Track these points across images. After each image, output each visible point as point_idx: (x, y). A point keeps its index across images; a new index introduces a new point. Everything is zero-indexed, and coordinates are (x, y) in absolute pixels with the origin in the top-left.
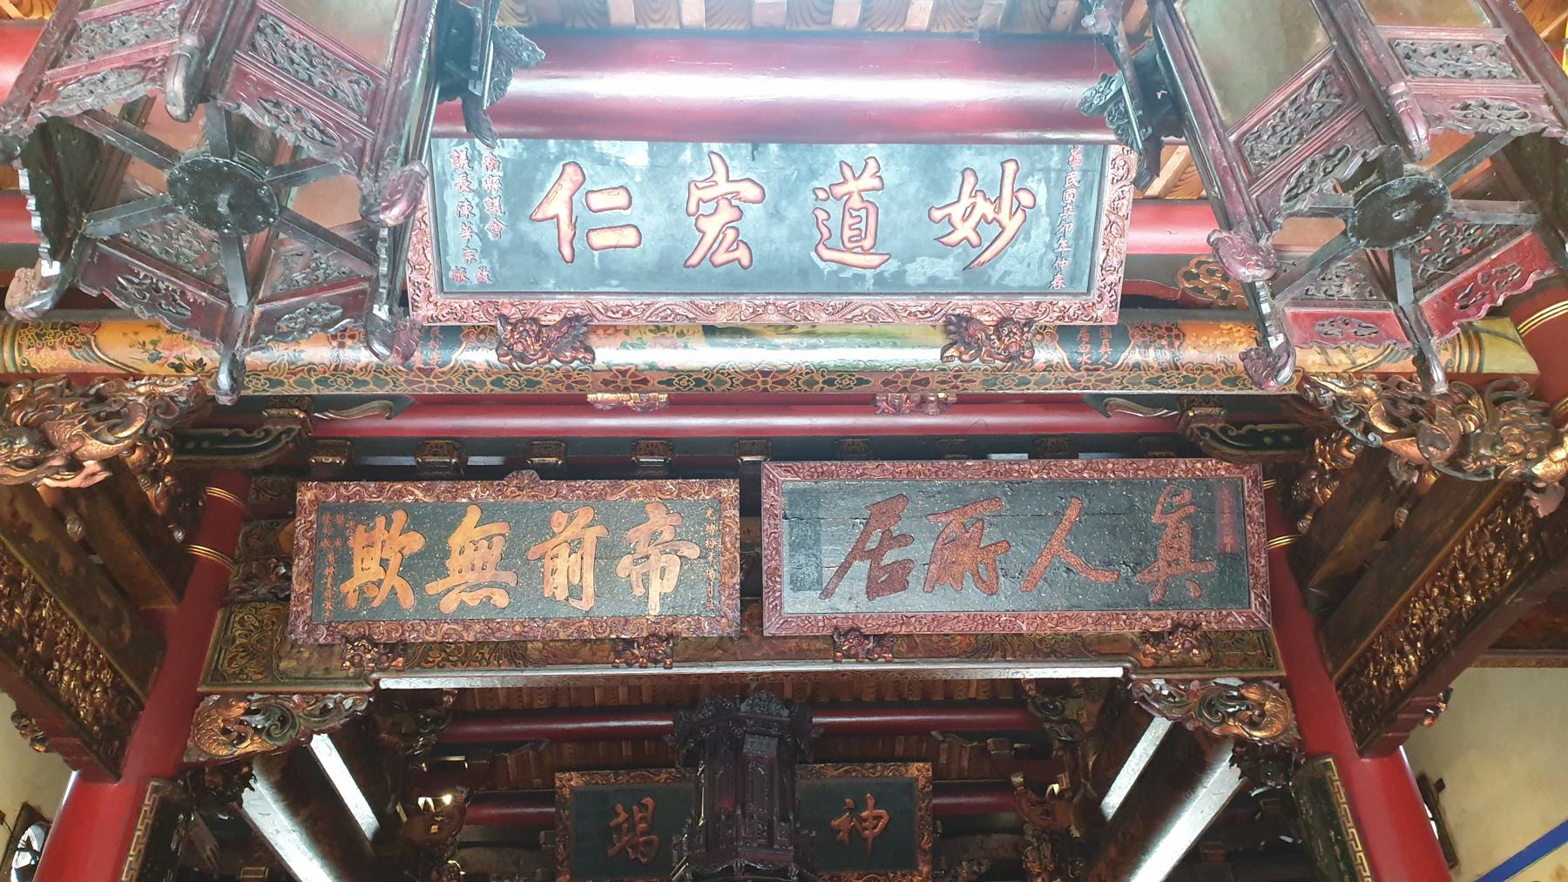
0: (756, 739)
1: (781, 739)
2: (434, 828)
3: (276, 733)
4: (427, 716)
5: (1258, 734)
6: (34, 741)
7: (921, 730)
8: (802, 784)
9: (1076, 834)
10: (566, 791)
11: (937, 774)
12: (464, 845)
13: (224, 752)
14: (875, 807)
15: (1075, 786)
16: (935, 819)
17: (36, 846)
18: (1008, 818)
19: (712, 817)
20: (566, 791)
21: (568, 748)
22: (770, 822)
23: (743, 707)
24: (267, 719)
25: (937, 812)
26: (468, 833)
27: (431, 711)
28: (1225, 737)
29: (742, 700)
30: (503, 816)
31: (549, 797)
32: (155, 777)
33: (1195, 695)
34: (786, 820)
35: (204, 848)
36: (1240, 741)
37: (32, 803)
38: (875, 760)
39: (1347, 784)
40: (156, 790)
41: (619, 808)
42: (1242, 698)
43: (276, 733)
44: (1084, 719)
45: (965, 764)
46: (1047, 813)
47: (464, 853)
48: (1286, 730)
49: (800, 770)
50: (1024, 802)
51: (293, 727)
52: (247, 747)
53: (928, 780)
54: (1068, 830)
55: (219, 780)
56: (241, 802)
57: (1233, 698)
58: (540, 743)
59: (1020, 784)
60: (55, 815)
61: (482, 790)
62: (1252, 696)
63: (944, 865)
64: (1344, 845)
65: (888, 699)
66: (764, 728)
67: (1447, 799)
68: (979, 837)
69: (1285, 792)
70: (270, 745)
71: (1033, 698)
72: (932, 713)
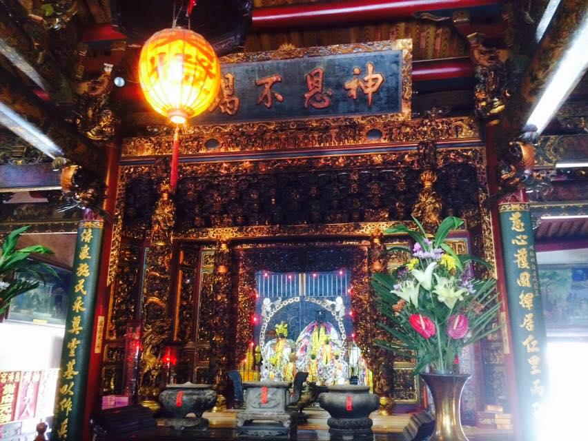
4: (61, 5)
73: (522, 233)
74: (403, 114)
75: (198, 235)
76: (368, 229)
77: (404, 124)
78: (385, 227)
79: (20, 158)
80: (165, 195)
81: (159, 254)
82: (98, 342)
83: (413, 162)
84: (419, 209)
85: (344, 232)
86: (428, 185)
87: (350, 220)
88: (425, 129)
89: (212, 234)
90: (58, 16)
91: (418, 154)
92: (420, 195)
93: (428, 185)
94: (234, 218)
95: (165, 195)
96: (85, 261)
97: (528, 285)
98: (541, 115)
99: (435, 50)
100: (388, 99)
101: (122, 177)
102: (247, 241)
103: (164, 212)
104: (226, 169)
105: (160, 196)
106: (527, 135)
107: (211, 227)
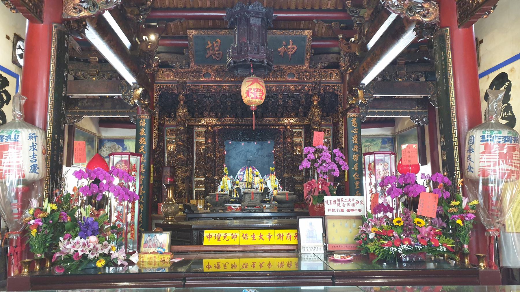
0: (254, 19)
1: (263, 19)
2: (149, 47)
3: (92, 9)
4: (142, 9)
5: (425, 20)
6: (11, 9)
7: (310, 19)
8: (269, 36)
9: (358, 54)
10: (191, 36)
11: (314, 35)
12: (159, 53)
13: (76, 15)
14: (292, 45)
15: (359, 38)
16: (312, 49)
17: (22, 47)
18: (336, 49)
19: (240, 44)
20: (191, 36)
21: (191, 22)
22: (258, 46)
23: (250, 7)
24: (88, 5)
25: (313, 47)
26: (160, 49)
27: (144, 7)
28: (413, 21)
29: (250, 5)
30: (171, 44)
31: (186, 38)
32: (55, 22)
33: (406, 5)
34: (263, 45)
35: (76, 47)
36: (419, 23)
37: (17, 33)
38: (293, 29)
39: (452, 37)
40: (56, 27)
41: (209, 42)
42: (422, 7)
43: (92, 9)
44: (365, 16)
45: (324, 31)
46: (349, 47)
47: (160, 55)
48: (435, 18)
49: (269, 32)
50: (342, 44)
51: (97, 7)
52: (83, 14)
53: (311, 36)
54: (355, 53)
55: (76, 25)
56: (85, 34)
57: (419, 7)
58: (181, 19)
59: (341, 38)
60: (24, 37)
61: (163, 35)
62: (426, 6)
63: (313, 64)
64: (448, 86)
65: (299, 8)
66: (257, 14)
67: (482, 47)
68: (325, 55)
69: (430, 40)
70: (90, 14)
71: (350, 8)
72: (314, 13)
73: (356, 128)
74: (306, 66)
75: (195, 122)
76: (285, 121)
77: (305, 71)
78: (293, 121)
79: (94, 76)
80: (182, 102)
81: (182, 133)
82: (152, 178)
83: (309, 90)
84: (311, 114)
85: (272, 122)
86: (315, 103)
87: (276, 116)
88: (316, 74)
89: (203, 121)
90: (142, 15)
91: (312, 87)
92: (312, 107)
93: (315, 103)
94: (216, 114)
95: (182, 102)
96: (143, 136)
97: (357, 151)
98: (366, 81)
99: (322, 33)
100: (297, 59)
101: (156, 90)
102: (220, 125)
103: (182, 112)
104: (215, 89)
105: (179, 102)
106: (361, 86)
107: (203, 117)
